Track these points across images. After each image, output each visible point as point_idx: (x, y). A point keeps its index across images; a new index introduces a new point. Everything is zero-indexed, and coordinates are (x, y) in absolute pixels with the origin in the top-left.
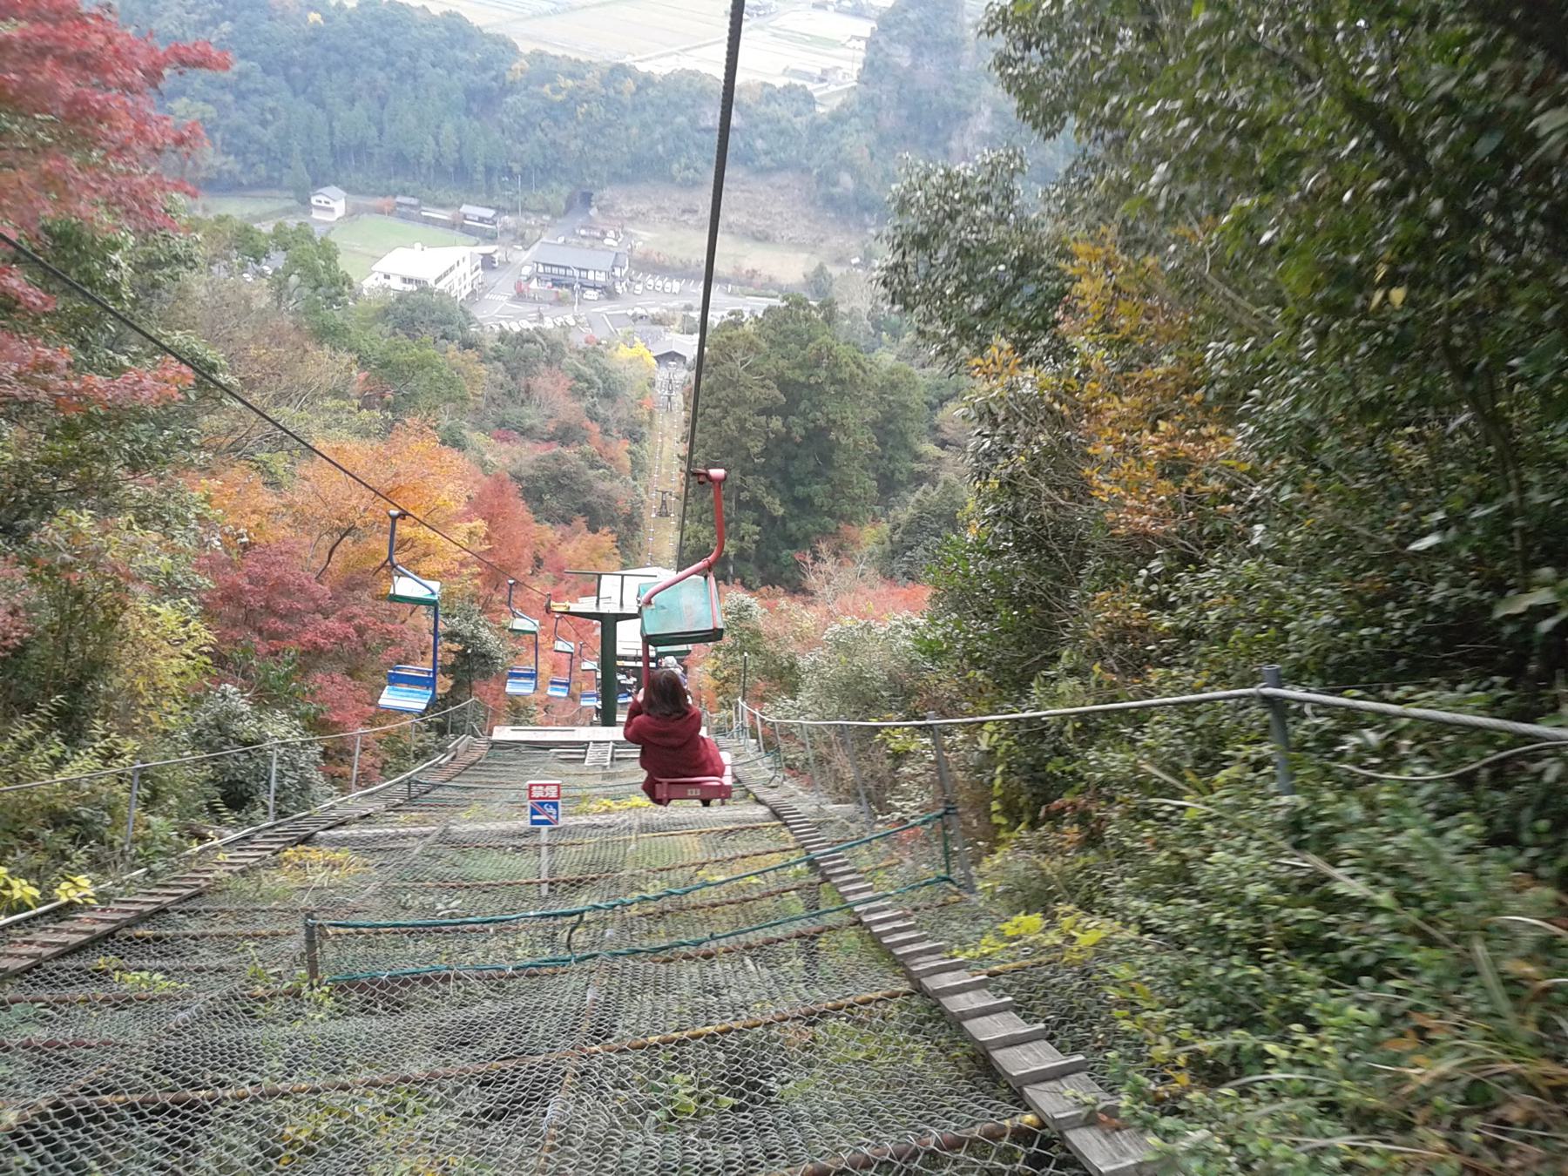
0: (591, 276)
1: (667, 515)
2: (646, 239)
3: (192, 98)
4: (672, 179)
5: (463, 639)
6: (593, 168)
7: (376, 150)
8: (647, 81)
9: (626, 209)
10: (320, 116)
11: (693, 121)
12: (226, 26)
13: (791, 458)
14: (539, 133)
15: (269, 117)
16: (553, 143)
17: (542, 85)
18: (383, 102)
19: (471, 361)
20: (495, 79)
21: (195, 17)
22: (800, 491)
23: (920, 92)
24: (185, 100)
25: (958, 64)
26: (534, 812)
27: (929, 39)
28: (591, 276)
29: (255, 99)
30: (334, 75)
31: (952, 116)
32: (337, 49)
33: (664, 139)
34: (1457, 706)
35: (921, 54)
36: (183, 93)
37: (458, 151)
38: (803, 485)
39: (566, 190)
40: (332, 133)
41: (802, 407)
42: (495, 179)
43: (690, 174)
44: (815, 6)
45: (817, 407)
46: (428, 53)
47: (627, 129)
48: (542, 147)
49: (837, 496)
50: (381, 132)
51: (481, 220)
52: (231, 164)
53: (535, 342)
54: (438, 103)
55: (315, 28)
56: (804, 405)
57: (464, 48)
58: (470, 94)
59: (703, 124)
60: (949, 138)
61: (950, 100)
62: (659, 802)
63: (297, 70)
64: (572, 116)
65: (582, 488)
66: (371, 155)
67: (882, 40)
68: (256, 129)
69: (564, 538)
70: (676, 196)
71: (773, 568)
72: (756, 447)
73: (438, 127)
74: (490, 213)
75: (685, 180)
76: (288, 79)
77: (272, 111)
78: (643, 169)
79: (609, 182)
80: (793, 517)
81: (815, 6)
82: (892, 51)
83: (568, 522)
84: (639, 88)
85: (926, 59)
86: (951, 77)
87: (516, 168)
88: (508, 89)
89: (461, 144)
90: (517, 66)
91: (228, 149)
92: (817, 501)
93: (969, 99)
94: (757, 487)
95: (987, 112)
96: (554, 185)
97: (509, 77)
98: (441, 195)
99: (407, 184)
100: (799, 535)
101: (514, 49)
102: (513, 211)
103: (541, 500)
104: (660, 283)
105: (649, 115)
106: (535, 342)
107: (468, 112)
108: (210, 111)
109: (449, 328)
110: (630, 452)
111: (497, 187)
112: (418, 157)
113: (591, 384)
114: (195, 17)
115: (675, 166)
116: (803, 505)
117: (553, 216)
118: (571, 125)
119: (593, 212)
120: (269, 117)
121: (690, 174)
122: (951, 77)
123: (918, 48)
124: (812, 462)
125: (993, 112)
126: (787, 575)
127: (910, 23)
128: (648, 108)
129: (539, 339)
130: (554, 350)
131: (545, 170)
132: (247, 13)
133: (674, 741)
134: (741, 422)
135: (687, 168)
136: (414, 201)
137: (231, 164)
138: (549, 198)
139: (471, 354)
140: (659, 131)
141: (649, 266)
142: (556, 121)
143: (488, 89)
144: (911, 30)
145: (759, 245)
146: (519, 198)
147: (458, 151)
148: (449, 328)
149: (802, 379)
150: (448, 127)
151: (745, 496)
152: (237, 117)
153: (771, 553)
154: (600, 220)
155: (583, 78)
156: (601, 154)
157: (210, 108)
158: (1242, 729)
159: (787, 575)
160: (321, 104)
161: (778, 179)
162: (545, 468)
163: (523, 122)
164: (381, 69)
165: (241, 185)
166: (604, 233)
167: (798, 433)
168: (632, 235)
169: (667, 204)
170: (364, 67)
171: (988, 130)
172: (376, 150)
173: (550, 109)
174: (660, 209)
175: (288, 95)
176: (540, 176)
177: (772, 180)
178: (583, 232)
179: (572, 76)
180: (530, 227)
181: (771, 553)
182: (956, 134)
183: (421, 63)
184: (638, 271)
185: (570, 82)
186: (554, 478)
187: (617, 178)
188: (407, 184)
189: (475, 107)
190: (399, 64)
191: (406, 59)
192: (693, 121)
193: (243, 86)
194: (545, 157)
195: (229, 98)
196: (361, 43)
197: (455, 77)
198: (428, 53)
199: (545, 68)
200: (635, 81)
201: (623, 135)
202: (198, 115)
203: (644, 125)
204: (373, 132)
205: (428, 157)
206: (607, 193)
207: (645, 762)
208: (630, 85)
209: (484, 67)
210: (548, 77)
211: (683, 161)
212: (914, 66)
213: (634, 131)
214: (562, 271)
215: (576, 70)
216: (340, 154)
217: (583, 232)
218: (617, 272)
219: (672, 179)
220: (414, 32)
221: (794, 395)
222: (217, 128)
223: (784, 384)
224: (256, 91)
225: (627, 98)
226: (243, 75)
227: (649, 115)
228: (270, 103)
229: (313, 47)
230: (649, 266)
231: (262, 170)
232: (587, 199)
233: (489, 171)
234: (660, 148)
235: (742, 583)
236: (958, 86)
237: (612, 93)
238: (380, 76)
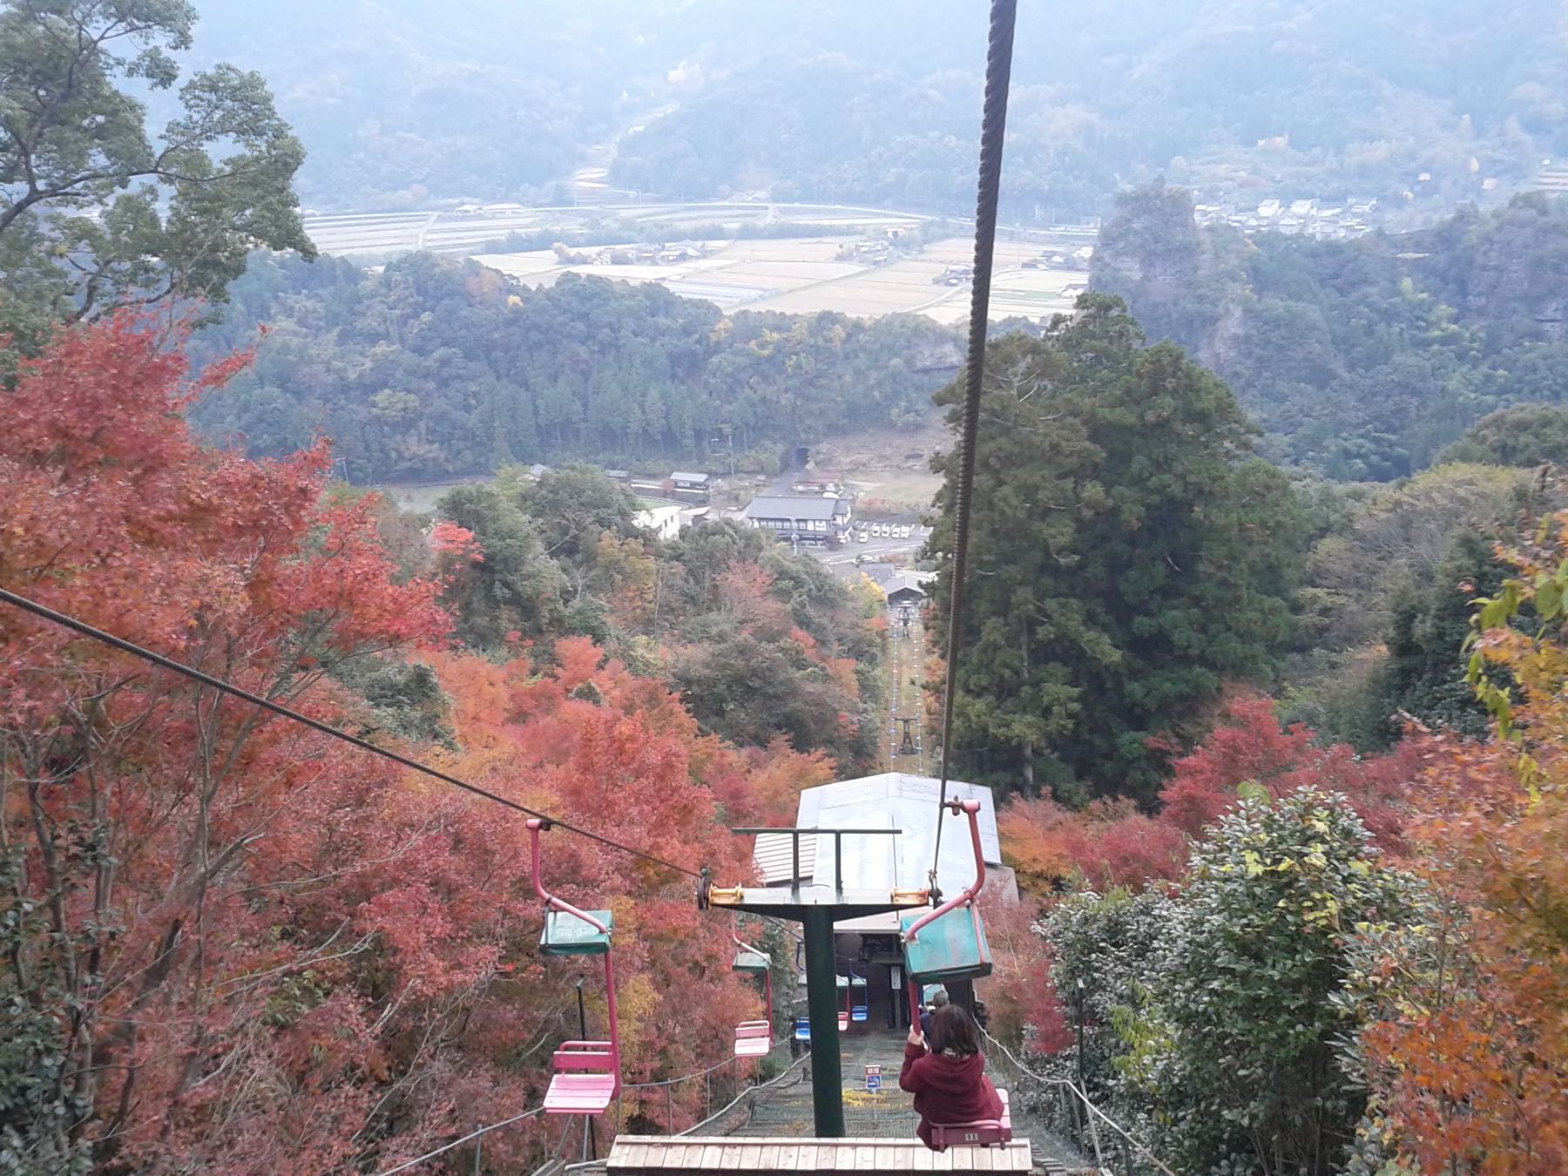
0: (810, 526)
1: (913, 752)
2: (867, 489)
3: (393, 388)
5: (192, 845)
6: (807, 422)
7: (582, 426)
8: (858, 327)
9: (845, 461)
10: (524, 396)
11: (909, 362)
12: (426, 317)
13: (1117, 567)
14: (747, 391)
15: (473, 402)
16: (764, 400)
17: (747, 343)
18: (586, 375)
19: (634, 553)
20: (699, 342)
21: (398, 312)
22: (1142, 624)
23: (1156, 305)
24: (387, 391)
25: (1196, 269)
27: (1160, 247)
28: (810, 526)
29: (457, 384)
30: (536, 355)
31: (1197, 324)
32: (537, 327)
33: (879, 384)
35: (1152, 265)
36: (385, 385)
37: (666, 418)
38: (1148, 613)
39: (780, 448)
40: (536, 413)
41: (1135, 468)
42: (705, 444)
43: (911, 417)
44: (1025, 266)
45: (1162, 465)
46: (630, 323)
47: (840, 377)
49: (1213, 628)
50: (585, 405)
51: (693, 485)
52: (435, 451)
53: (723, 534)
54: (641, 371)
55: (516, 310)
56: (1139, 463)
57: (667, 314)
58: (674, 359)
59: (920, 365)
60: (1196, 349)
61: (1190, 306)
62: (935, 1148)
63: (498, 354)
64: (781, 370)
65: (780, 690)
66: (578, 430)
67: (1107, 255)
68: (460, 415)
69: (756, 763)
70: (898, 442)
71: (1108, 767)
72: (1060, 533)
73: (643, 395)
74: (701, 478)
75: (907, 424)
76: (492, 364)
77: (475, 395)
78: (862, 418)
79: (826, 435)
80: (1134, 674)
81: (1025, 266)
82: (1119, 265)
83: (763, 743)
84: (849, 336)
85: (1159, 270)
86: (1189, 285)
87: (727, 429)
88: (716, 349)
90: (720, 325)
91: (432, 436)
92: (1178, 638)
93: (1214, 304)
94: (1068, 617)
95: (1238, 312)
96: (768, 444)
97: (713, 338)
98: (650, 465)
99: (616, 458)
100: (1152, 705)
101: (717, 311)
102: (723, 476)
103: (721, 713)
104: (886, 529)
105: (862, 361)
106: (723, 534)
107: (673, 377)
108: (413, 400)
109: (603, 512)
110: (858, 672)
111: (708, 451)
112: (624, 428)
113: (799, 583)
114: (398, 312)
115: (895, 411)
116: (1151, 650)
117: (768, 476)
118: (780, 380)
119: (810, 466)
120: (473, 402)
121: (911, 417)
122: (1189, 285)
123: (1149, 259)
124: (1160, 570)
125: (1245, 311)
126: (1135, 776)
127: (1137, 233)
129: (727, 529)
130: (750, 545)
131: (755, 429)
132: (446, 301)
133: (958, 1089)
134: (1028, 492)
136: (623, 474)
137: (435, 451)
138: (763, 457)
139: (633, 544)
140: (873, 377)
141: (872, 514)
142: (765, 377)
143: (693, 354)
144: (1138, 241)
146: (732, 460)
147: (666, 418)
148: (603, 512)
149: (1131, 419)
150: (654, 394)
151: (1045, 632)
152: (440, 404)
153: (1098, 741)
154: (817, 472)
155: (789, 330)
156: (814, 407)
157: (412, 397)
158: (327, 985)
159: (1135, 776)
160: (525, 384)
162: (724, 666)
163: (729, 381)
164: (583, 343)
165: (448, 472)
166: (823, 487)
167: (1133, 514)
168: (853, 487)
170: (565, 343)
171: (1240, 332)
172: (582, 426)
173: (757, 364)
174: (882, 457)
175: (491, 378)
178: (801, 488)
179: (777, 329)
180: (745, 488)
181: (1098, 741)
182: (1203, 343)
183: (623, 332)
184: (862, 520)
185: (776, 336)
186: (739, 680)
187: (834, 430)
188: (616, 458)
189: (680, 372)
190: (600, 336)
191: (607, 330)
192: (909, 362)
193: (446, 372)
195: (431, 385)
196: (560, 319)
197: (658, 343)
198: (630, 323)
199: (749, 326)
200: (844, 327)
202: (400, 405)
203: (857, 372)
204: (577, 406)
205: (635, 427)
206: (824, 447)
207: (919, 1105)
208: (839, 331)
209: (686, 332)
210: (754, 333)
211: (903, 404)
212: (1146, 278)
213: (847, 378)
214: (779, 524)
215: (781, 323)
216: (545, 433)
217: (801, 488)
218: (839, 521)
219: (892, 425)
220: (614, 304)
221: (1117, 448)
222: (420, 417)
223: (1098, 432)
224: (459, 377)
225: (837, 346)
226: (445, 362)
227: (862, 361)
228: (474, 388)
229: (514, 329)
230: (872, 514)
231: (468, 456)
232: (803, 456)
233: (699, 435)
234: (876, 393)
235: (1056, 797)
236: (1200, 291)
237: (821, 342)
238: (582, 351)
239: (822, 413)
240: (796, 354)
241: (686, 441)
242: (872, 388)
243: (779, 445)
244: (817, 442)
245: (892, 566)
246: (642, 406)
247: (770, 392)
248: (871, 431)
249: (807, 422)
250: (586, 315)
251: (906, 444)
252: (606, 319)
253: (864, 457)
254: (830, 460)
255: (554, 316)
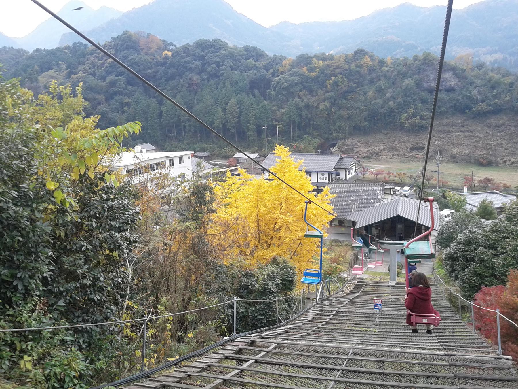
4: (402, 127)
6: (338, 124)
14: (296, 99)
26: (375, 306)
34: (389, 381)
37: (239, 117)
48: (298, 108)
55: (166, 58)
70: (405, 139)
75: (413, 125)
77: (128, 104)
79: (351, 134)
89: (241, 112)
105: (382, 83)
121: (417, 120)
128: (382, 78)
135: (414, 116)
142: (311, 91)
145: (483, 169)
150: (233, 101)
156: (344, 113)
161: (494, 120)
169: (397, 144)
176: (298, 133)
177: (489, 121)
185: (321, 63)
191: (214, 66)
194: (300, 116)
201: (362, 98)
209: (267, 68)
211: (411, 111)
233: (259, 132)
239: (349, 118)
240: (335, 75)
241: (250, 133)
242: (389, 100)
243: (316, 140)
244: (345, 138)
245: (378, 188)
246: (224, 110)
247: (312, 100)
248: (385, 132)
249: (338, 124)
250: (203, 57)
251: (412, 140)
252: (215, 59)
253: (377, 149)
254: (352, 150)
255: (183, 57)
